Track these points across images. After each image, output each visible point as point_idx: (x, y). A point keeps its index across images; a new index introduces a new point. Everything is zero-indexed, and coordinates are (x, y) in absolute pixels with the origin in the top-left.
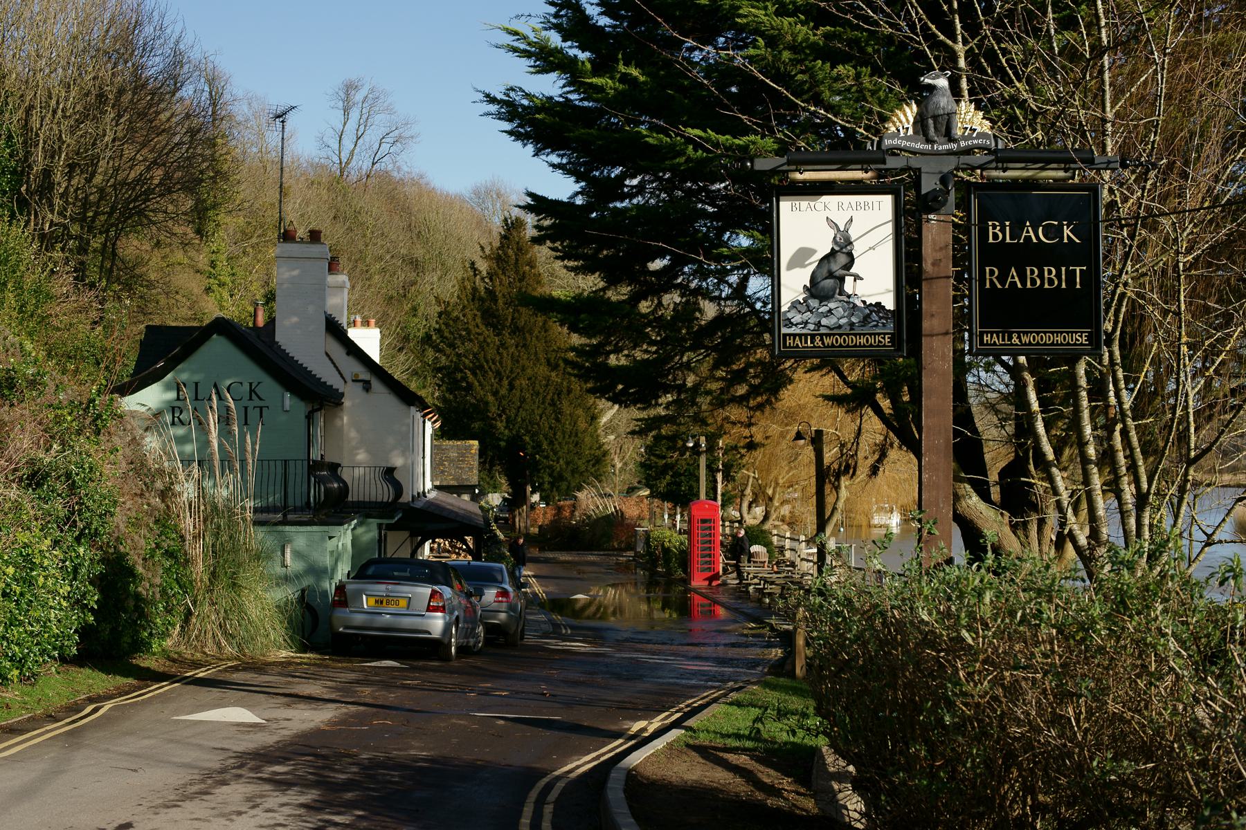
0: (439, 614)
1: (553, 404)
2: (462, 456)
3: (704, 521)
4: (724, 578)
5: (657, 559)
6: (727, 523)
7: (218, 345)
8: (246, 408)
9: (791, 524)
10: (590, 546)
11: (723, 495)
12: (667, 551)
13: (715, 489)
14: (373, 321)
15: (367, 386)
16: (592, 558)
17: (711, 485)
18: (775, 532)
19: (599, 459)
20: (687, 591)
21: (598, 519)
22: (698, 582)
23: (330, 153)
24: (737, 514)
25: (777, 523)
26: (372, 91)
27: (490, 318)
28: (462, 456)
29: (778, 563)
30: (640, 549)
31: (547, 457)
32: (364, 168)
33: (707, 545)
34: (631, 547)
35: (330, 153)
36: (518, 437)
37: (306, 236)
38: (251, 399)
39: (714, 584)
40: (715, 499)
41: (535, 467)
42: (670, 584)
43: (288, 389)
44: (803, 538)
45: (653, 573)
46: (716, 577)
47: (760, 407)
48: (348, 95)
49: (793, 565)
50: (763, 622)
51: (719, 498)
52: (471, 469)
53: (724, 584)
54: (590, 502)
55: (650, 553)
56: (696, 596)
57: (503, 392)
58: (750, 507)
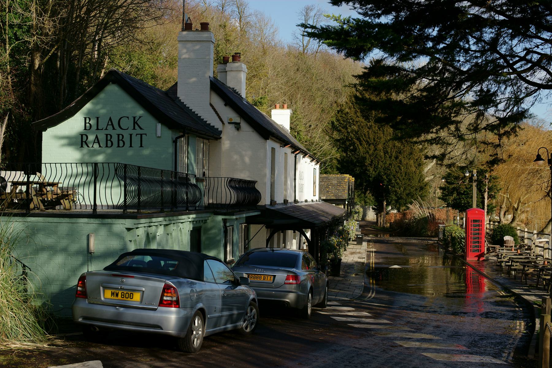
0: (173, 309)
2: (340, 183)
3: (475, 221)
4: (487, 255)
5: (448, 244)
6: (492, 223)
7: (112, 89)
8: (131, 135)
9: (527, 224)
10: (417, 234)
11: (488, 206)
12: (453, 239)
13: (483, 203)
15: (238, 126)
16: (414, 241)
17: (480, 200)
18: (519, 228)
19: (423, 187)
20: (464, 264)
21: (423, 218)
22: (471, 259)
23: (298, 41)
24: (498, 218)
25: (519, 223)
26: (318, 11)
28: (340, 183)
29: (521, 247)
30: (441, 236)
32: (315, 48)
33: (477, 236)
34: (437, 235)
35: (298, 41)
37: (199, 27)
38: (134, 129)
39: (481, 259)
40: (483, 208)
41: (388, 192)
42: (455, 259)
43: (160, 121)
44: (535, 232)
45: (447, 251)
46: (482, 255)
47: (507, 134)
48: (307, 13)
49: (529, 248)
50: (510, 292)
51: (486, 208)
52: (344, 190)
53: (487, 260)
54: (417, 211)
55: (445, 240)
56: (470, 269)
58: (505, 214)
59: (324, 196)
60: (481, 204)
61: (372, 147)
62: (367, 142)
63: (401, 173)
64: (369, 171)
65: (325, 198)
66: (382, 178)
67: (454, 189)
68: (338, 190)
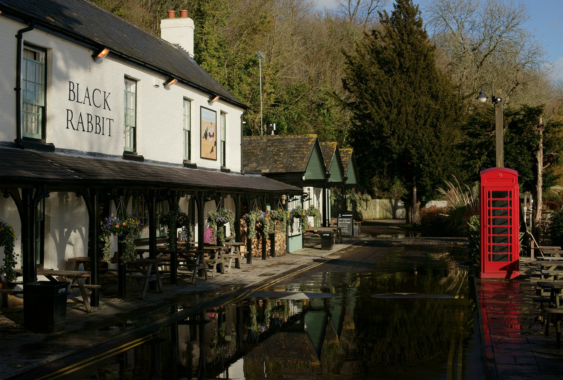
1: (435, 126)
3: (497, 194)
11: (544, 175)
14: (185, 12)
23: (344, 9)
27: (383, 63)
31: (428, 165)
35: (344, 9)
36: (406, 151)
57: (393, 117)
59: (268, 168)
60: (531, 172)
61: (395, 111)
62: (389, 104)
63: (440, 146)
64: (390, 144)
65: (267, 171)
66: (410, 153)
67: (481, 145)
68: (293, 158)
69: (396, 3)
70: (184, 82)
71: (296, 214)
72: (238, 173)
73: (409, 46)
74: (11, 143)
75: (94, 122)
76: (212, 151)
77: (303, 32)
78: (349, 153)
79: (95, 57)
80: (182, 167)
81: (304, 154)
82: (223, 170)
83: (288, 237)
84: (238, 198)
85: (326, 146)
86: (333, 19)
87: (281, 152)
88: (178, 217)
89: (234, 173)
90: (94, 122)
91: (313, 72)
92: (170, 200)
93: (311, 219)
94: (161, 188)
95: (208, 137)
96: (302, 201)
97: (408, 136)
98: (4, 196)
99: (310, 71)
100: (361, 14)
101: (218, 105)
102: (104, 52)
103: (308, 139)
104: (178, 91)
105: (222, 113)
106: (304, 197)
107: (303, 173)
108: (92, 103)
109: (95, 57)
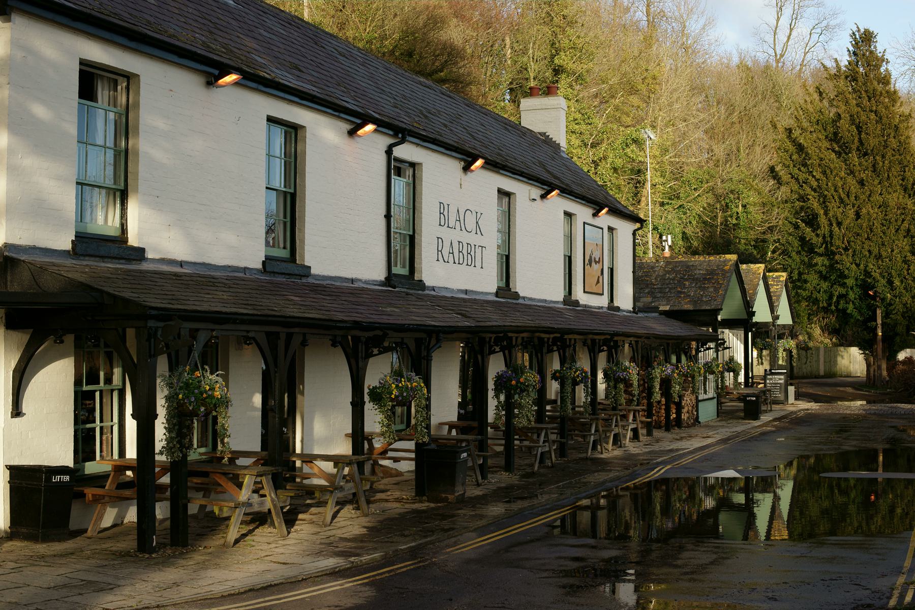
61: (851, 213)
65: (667, 308)
69: (851, 49)
70: (567, 192)
71: (709, 368)
72: (630, 312)
73: (873, 116)
74: (381, 281)
75: (465, 252)
76: (598, 282)
77: (701, 85)
78: (781, 279)
79: (466, 169)
80: (562, 306)
81: (718, 283)
82: (506, 290)
83: (698, 401)
84: (637, 346)
85: (749, 271)
86: (750, 64)
87: (687, 280)
88: (575, 372)
89: (624, 311)
90: (465, 252)
91: (720, 151)
92: (507, 352)
93: (729, 377)
94: (552, 336)
95: (593, 264)
96: (717, 351)
97: (869, 251)
98: (332, 345)
99: (716, 151)
100: (794, 54)
101: (605, 219)
102: (479, 162)
103: (725, 261)
104: (557, 203)
105: (611, 229)
106: (721, 345)
107: (717, 311)
108: (463, 228)
109: (466, 169)
